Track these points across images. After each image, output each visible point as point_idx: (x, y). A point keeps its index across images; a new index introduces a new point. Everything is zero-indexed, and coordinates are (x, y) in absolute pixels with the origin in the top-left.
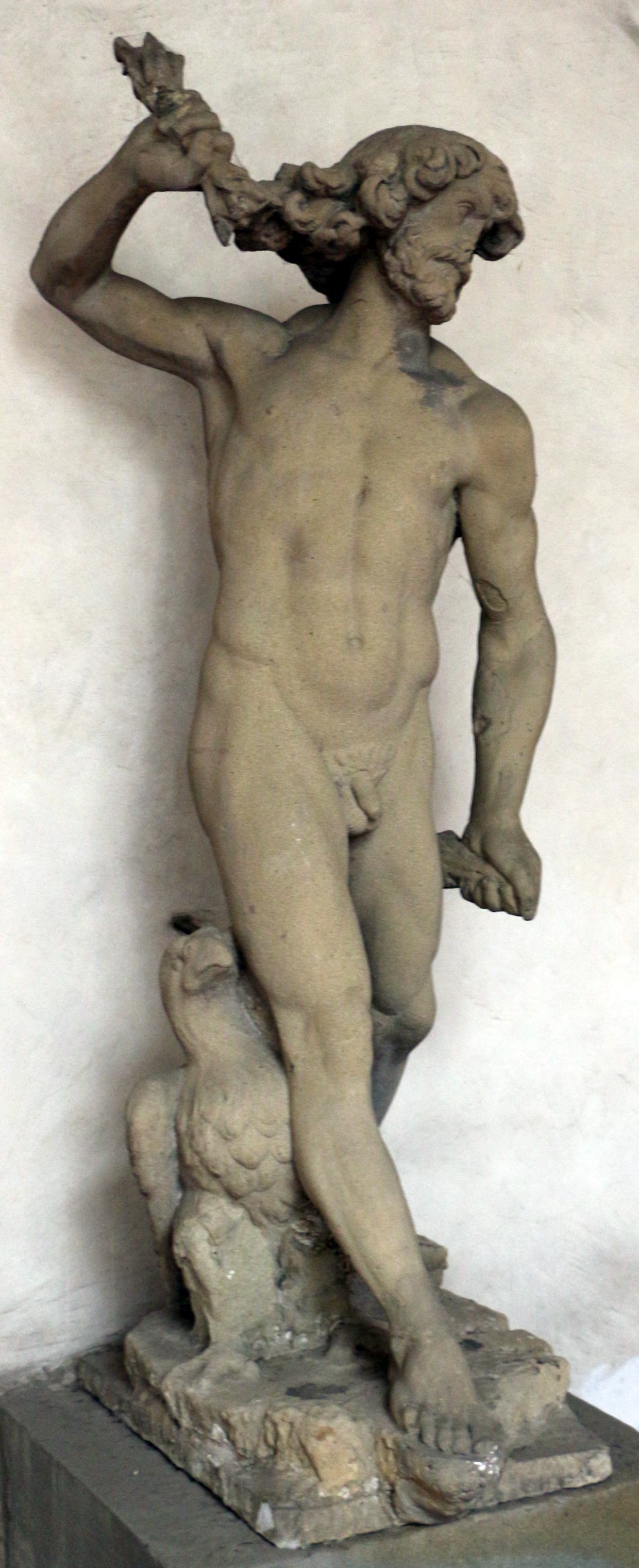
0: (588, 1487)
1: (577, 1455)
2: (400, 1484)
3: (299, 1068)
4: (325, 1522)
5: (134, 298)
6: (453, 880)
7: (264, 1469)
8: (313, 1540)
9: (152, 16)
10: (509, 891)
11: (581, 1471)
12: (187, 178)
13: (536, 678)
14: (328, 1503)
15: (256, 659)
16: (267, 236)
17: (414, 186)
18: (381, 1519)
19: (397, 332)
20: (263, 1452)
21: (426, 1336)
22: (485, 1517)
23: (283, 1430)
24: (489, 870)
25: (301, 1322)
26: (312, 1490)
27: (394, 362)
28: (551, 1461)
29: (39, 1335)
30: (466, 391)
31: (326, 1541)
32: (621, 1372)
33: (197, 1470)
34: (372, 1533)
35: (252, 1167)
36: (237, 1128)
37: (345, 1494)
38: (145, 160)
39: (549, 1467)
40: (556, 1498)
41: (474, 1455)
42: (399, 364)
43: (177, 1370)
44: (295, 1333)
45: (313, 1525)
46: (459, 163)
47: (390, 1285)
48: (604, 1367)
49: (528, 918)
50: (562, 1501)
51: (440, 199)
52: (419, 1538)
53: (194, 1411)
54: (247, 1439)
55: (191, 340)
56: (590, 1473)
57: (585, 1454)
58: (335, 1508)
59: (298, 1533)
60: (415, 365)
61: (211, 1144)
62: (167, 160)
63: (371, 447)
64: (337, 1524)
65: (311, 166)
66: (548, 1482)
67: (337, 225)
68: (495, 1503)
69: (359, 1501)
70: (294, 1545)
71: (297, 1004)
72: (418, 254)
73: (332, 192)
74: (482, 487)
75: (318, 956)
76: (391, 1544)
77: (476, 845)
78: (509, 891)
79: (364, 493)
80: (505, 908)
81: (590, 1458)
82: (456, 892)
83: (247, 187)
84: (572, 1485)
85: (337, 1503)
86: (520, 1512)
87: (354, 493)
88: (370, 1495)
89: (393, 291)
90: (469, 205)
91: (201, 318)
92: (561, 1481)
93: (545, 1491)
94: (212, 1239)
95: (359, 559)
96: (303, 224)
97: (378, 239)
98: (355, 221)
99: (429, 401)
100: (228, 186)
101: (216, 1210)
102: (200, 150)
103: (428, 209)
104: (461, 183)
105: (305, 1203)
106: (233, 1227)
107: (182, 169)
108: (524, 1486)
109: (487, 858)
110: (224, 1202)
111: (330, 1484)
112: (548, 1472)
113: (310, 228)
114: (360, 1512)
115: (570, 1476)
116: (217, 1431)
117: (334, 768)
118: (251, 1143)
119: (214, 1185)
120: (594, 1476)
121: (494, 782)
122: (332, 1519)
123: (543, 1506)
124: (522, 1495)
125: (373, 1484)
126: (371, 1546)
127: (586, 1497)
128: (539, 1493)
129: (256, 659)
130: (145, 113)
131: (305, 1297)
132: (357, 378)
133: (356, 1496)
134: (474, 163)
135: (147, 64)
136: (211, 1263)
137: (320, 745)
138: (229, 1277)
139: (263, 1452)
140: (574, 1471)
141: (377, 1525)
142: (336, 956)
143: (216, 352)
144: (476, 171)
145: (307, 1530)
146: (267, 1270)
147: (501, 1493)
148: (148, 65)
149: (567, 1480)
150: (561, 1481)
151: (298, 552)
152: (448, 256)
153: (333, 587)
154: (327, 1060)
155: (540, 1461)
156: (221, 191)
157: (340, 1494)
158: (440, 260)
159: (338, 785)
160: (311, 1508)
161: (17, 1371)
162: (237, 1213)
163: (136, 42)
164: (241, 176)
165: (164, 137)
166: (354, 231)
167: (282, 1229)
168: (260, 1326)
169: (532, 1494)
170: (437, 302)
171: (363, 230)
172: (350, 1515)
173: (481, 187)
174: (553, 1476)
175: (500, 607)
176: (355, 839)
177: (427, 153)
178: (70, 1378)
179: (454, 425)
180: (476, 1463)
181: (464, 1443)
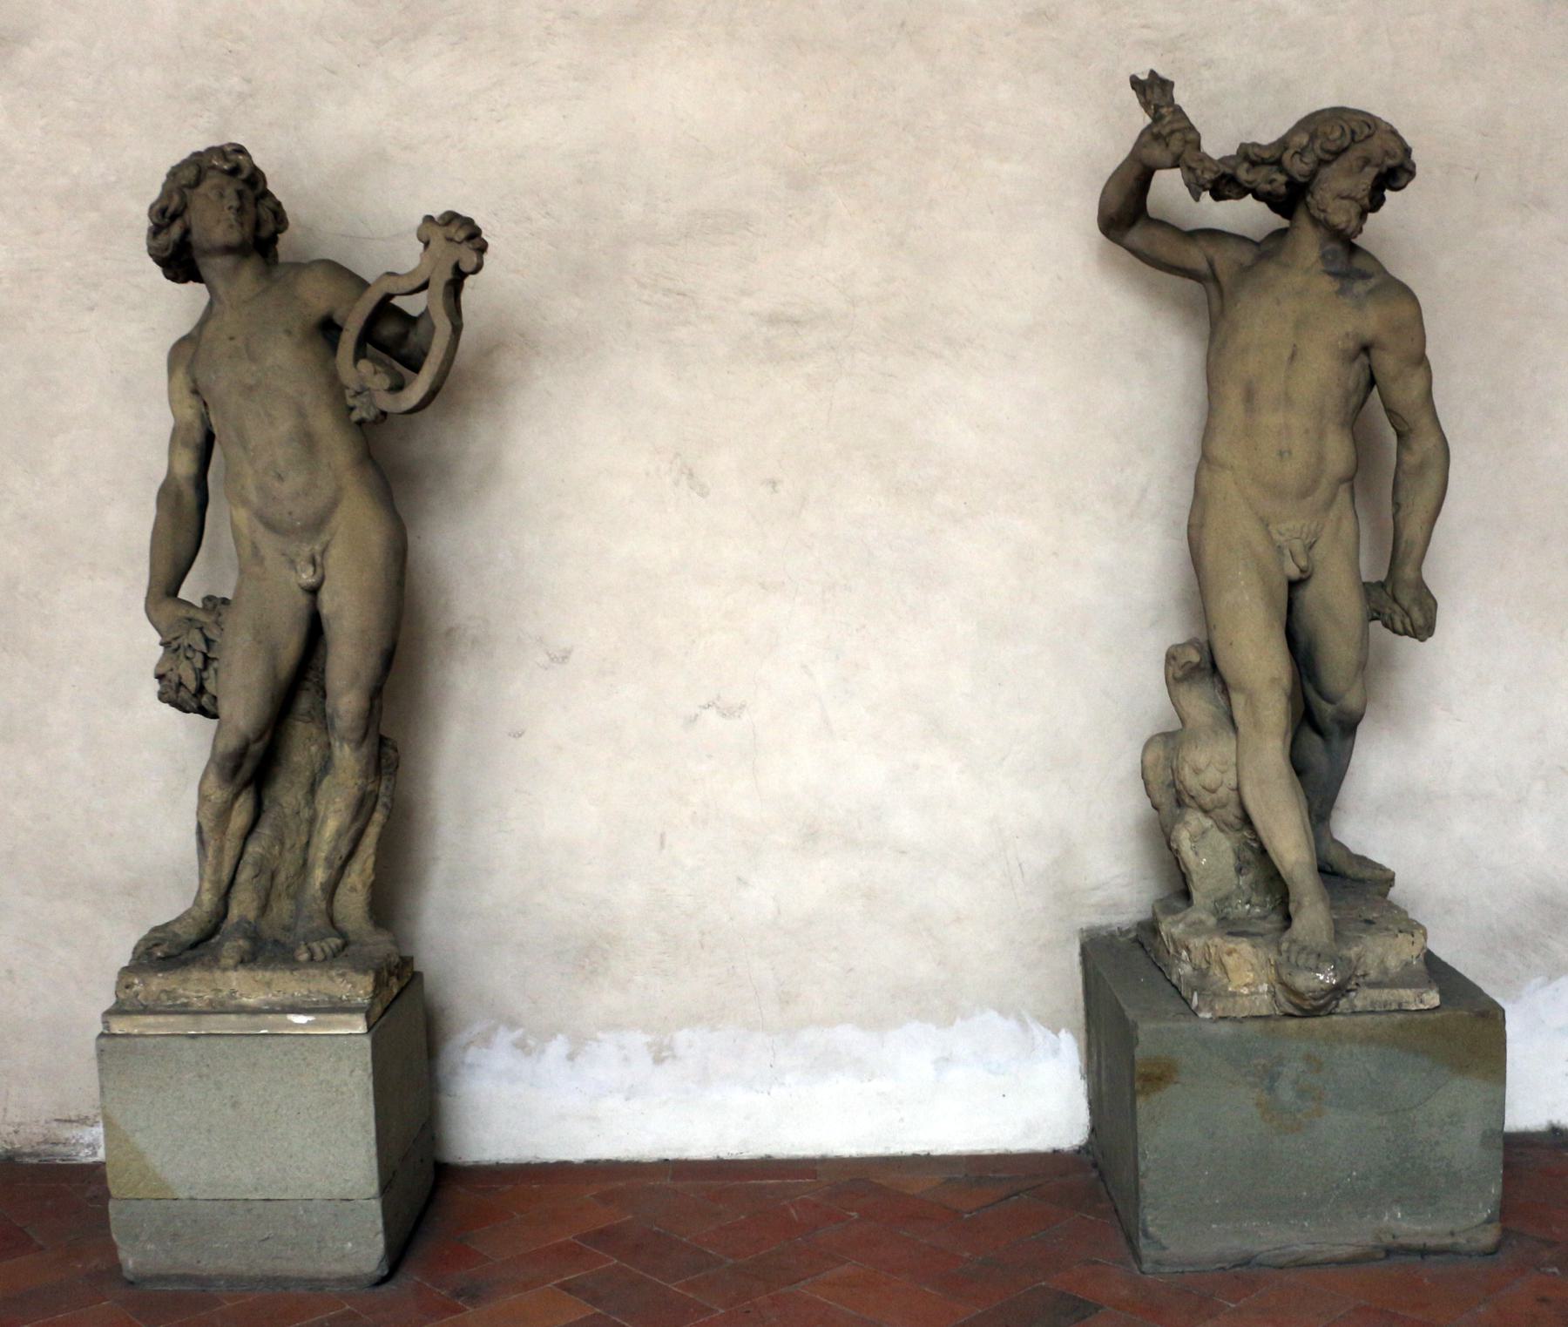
2: (1278, 986)
3: (1241, 729)
4: (1230, 1005)
5: (1158, 234)
6: (1375, 615)
7: (1202, 974)
8: (1220, 1014)
10: (1407, 621)
12: (1169, 160)
13: (1433, 477)
14: (1234, 994)
15: (1222, 466)
17: (1319, 152)
19: (1322, 247)
20: (1204, 966)
21: (1306, 901)
22: (1341, 1018)
23: (1212, 950)
24: (1396, 607)
25: (1254, 899)
26: (1226, 987)
27: (1320, 266)
29: (1116, 906)
30: (1373, 282)
32: (1555, 984)
33: (1174, 980)
35: (1214, 791)
36: (1202, 767)
37: (1245, 991)
38: (1145, 153)
41: (1317, 970)
43: (1169, 919)
44: (1252, 906)
46: (1353, 132)
47: (1289, 868)
48: (1539, 980)
50: (1399, 1017)
51: (1341, 159)
52: (1292, 1024)
53: (1174, 942)
54: (1198, 959)
55: (1195, 256)
59: (1212, 1009)
60: (1336, 267)
61: (1191, 781)
62: (1157, 152)
63: (1300, 324)
65: (1254, 145)
67: (1271, 182)
70: (1208, 1015)
71: (1242, 690)
72: (1328, 196)
74: (1383, 348)
75: (1251, 657)
76: (1272, 1024)
77: (1389, 589)
78: (1407, 621)
79: (1293, 357)
80: (1406, 633)
82: (1378, 623)
83: (1207, 164)
86: (1368, 1018)
87: (1286, 354)
89: (1316, 222)
91: (1203, 243)
94: (1192, 838)
95: (1287, 400)
97: (1330, 178)
98: (1281, 178)
99: (1342, 292)
100: (1193, 165)
101: (1195, 820)
102: (1176, 144)
103: (1334, 166)
104: (1359, 147)
105: (1247, 820)
106: (1204, 832)
107: (1167, 158)
108: (1373, 1003)
109: (1395, 600)
110: (1199, 814)
111: (1235, 983)
116: (1184, 953)
117: (1276, 537)
118: (1211, 777)
119: (1192, 804)
121: (1402, 546)
125: (1265, 987)
126: (1258, 1025)
127: (1417, 1016)
129: (1222, 466)
130: (1148, 120)
131: (1256, 883)
132: (1296, 279)
133: (1252, 993)
134: (1366, 131)
135: (1153, 90)
136: (1191, 853)
137: (1265, 523)
139: (1204, 966)
141: (1264, 1012)
143: (1211, 264)
144: (1369, 136)
146: (1229, 860)
148: (1148, 92)
150: (1400, 1004)
151: (1249, 396)
153: (1271, 419)
154: (1257, 725)
156: (1190, 169)
159: (1280, 549)
161: (1101, 928)
162: (1208, 823)
163: (1144, 77)
164: (1207, 158)
165: (1157, 137)
167: (1239, 835)
168: (1227, 898)
170: (1342, 226)
171: (1287, 184)
172: (1247, 1003)
173: (1375, 146)
176: (1294, 585)
177: (1328, 130)
178: (1132, 935)
179: (1360, 307)
181: (1312, 962)
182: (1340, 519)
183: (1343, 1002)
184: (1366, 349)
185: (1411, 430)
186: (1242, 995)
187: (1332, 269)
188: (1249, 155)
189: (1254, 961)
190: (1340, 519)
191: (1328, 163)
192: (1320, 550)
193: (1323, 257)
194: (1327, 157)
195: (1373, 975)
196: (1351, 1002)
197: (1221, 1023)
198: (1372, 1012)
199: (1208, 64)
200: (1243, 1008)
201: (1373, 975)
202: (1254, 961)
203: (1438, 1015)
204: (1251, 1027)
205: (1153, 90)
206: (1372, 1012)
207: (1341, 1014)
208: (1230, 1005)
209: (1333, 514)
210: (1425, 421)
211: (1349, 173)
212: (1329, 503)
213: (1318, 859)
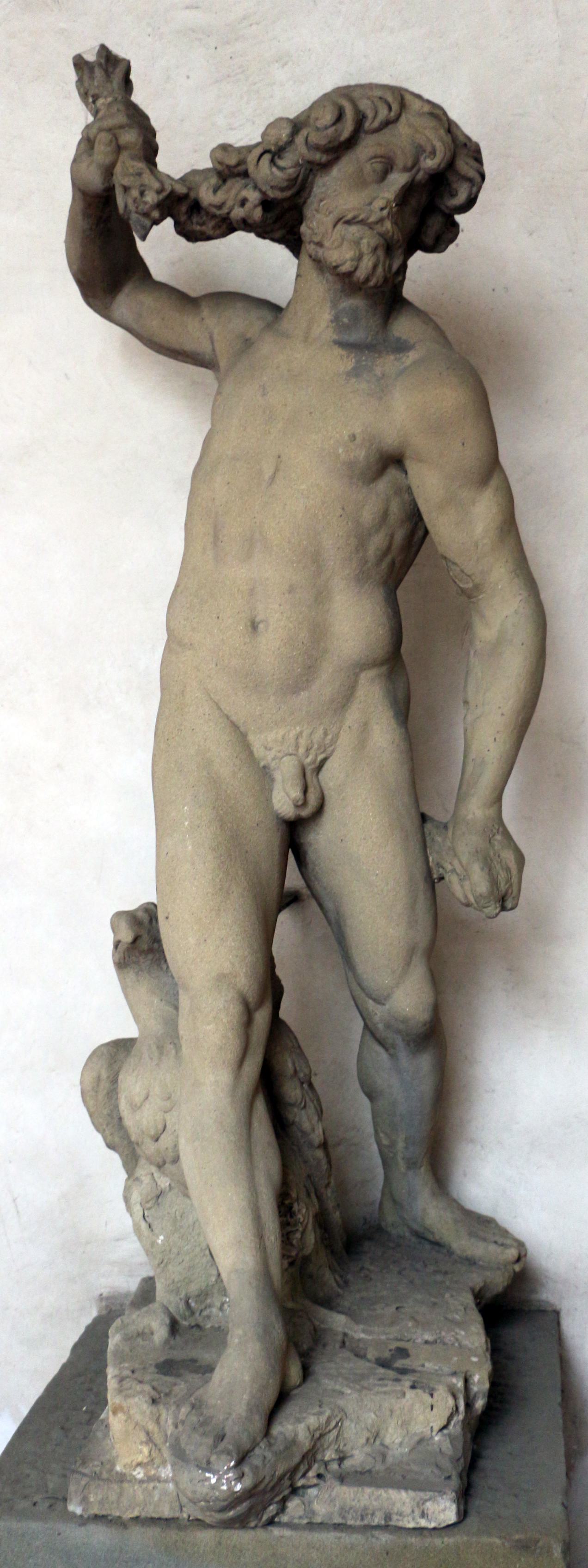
0: (419, 1531)
1: (412, 1493)
4: (113, 1497)
8: (95, 1510)
9: (257, 24)
11: (413, 1511)
14: (122, 1478)
16: (202, 224)
17: (303, 150)
18: (171, 1508)
19: (334, 305)
22: (287, 1533)
28: (382, 1492)
31: (110, 1515)
34: (160, 1519)
37: (139, 1473)
39: (378, 1498)
40: (376, 1533)
42: (335, 337)
45: (100, 1497)
49: (119, 915)
50: (385, 1538)
52: (206, 1537)
56: (423, 1515)
57: (422, 1495)
58: (126, 1485)
60: (357, 335)
64: (125, 1502)
66: (373, 1514)
68: (305, 1521)
69: (151, 1485)
70: (79, 1511)
73: (235, 171)
76: (173, 1535)
81: (426, 1501)
84: (400, 1524)
85: (130, 1481)
86: (329, 1537)
88: (166, 1481)
90: (383, 160)
92: (388, 1517)
93: (366, 1522)
96: (220, 207)
97: (381, 195)
99: (356, 372)
103: (335, 171)
108: (343, 1511)
112: (375, 1503)
113: (225, 211)
114: (151, 1495)
115: (400, 1514)
120: (430, 1521)
122: (121, 1495)
123: (356, 1538)
124: (337, 1520)
126: (154, 1532)
127: (413, 1540)
128: (358, 1523)
133: (150, 1479)
138: (159, 1242)
140: (407, 1510)
141: (167, 1513)
142: (209, 941)
144: (387, 124)
145: (92, 1500)
147: (313, 1513)
149: (395, 1517)
150: (388, 1517)
152: (354, 218)
155: (368, 1490)
157: (135, 1473)
158: (348, 222)
160: (103, 1480)
163: (91, 57)
166: (255, 206)
169: (350, 1522)
172: (140, 1497)
173: (403, 136)
174: (380, 1509)
175: (467, 583)
180: (207, 1475)
182: (365, 728)
183: (294, 1505)
184: (392, 461)
185: (477, 587)
186: (133, 1480)
187: (346, 338)
188: (230, 167)
189: (151, 1426)
190: (365, 728)
191: (325, 167)
192: (331, 776)
193: (336, 319)
194: (323, 158)
195: (358, 1458)
196: (307, 1505)
197: (92, 1527)
198: (338, 1527)
199: (283, 60)
200: (133, 1502)
201: (358, 1458)
202: (151, 1426)
203: (449, 1540)
204: (138, 1536)
205: (105, 75)
206: (338, 1527)
207: (289, 1525)
208: (113, 1497)
209: (353, 716)
210: (499, 574)
211: (360, 182)
212: (345, 698)
213: (447, 1194)
